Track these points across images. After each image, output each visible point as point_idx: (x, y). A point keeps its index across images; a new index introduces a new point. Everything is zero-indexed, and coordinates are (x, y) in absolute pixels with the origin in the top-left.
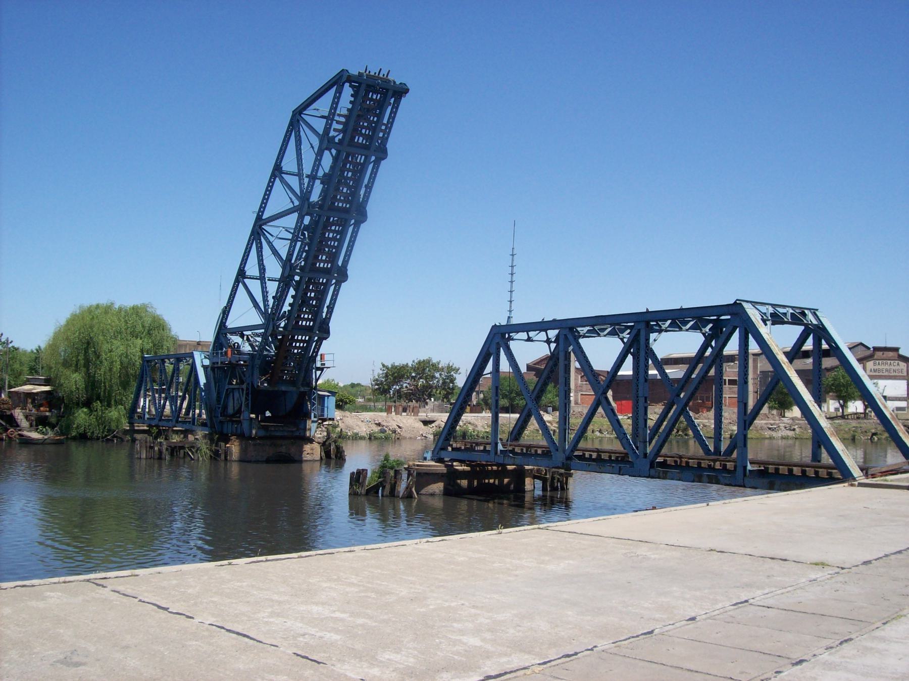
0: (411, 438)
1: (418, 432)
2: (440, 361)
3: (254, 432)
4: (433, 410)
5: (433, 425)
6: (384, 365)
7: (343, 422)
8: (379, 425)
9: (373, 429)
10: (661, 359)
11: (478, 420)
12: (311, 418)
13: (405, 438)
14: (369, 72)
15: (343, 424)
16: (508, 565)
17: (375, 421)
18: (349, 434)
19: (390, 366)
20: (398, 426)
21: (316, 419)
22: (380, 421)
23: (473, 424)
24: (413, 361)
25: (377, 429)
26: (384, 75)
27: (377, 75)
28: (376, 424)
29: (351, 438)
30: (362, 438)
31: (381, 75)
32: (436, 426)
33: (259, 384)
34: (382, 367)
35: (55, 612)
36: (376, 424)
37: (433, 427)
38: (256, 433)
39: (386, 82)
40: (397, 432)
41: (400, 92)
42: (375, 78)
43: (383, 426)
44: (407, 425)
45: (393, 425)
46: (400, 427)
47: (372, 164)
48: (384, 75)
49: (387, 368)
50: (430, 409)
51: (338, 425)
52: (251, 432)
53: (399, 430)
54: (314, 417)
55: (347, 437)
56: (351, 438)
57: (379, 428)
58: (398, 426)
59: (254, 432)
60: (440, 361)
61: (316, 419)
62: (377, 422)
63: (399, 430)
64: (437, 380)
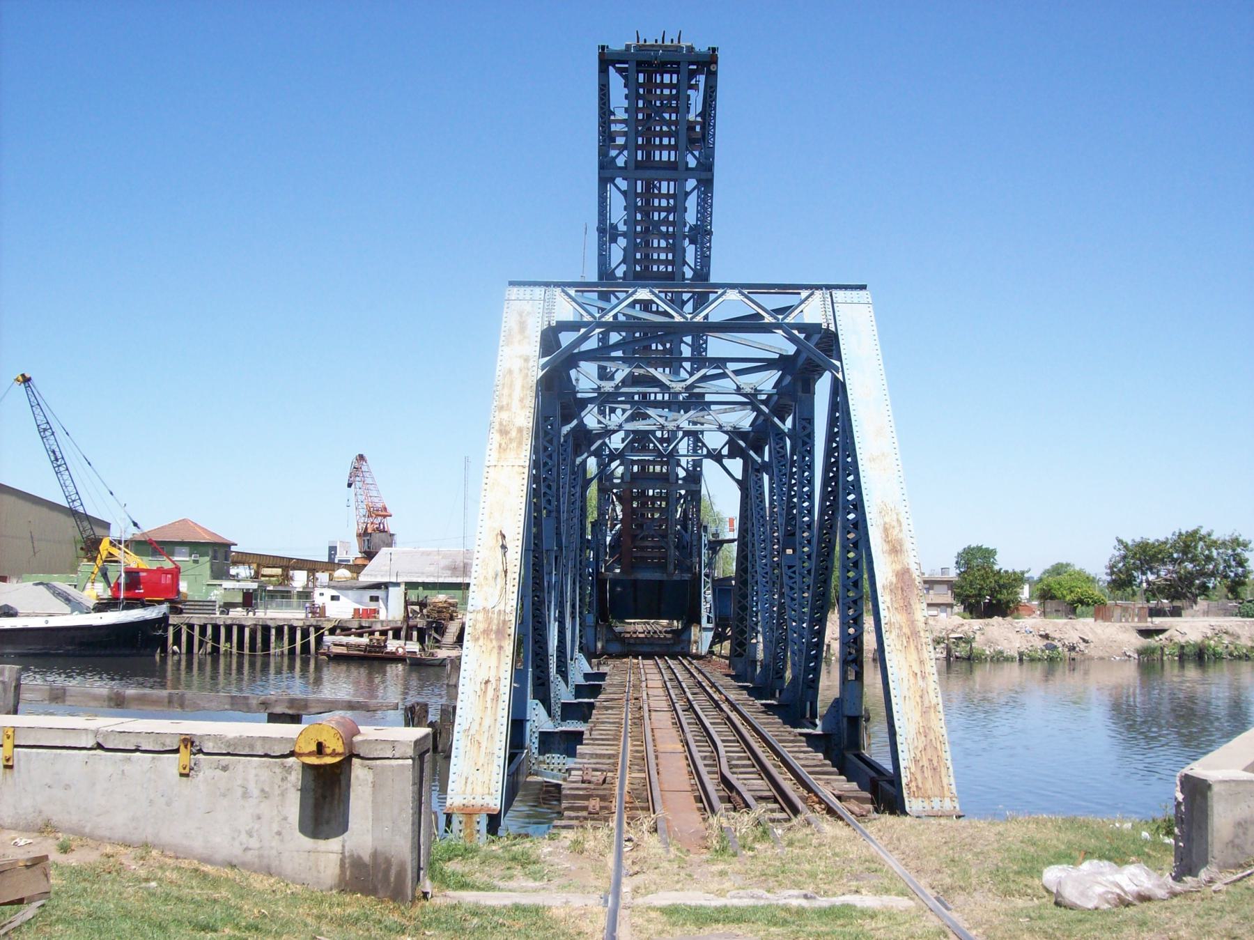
0: (1102, 659)
1: (1120, 647)
2: (1212, 531)
3: (599, 645)
4: (1208, 612)
5: (1161, 636)
6: (1120, 542)
7: (983, 634)
8: (1046, 637)
9: (1034, 644)
10: (750, 426)
11: (1243, 627)
12: (699, 622)
13: (1091, 658)
14: (645, 41)
15: (982, 637)
16: (845, 880)
17: (1039, 630)
18: (988, 653)
19: (1130, 543)
20: (1081, 638)
21: (710, 626)
22: (1047, 632)
23: (1232, 635)
24: (1173, 535)
25: (1040, 643)
26: (672, 41)
27: (660, 42)
28: (1041, 636)
29: (989, 659)
30: (1009, 659)
31: (667, 43)
32: (1166, 639)
33: (603, 570)
34: (1116, 543)
35: (732, 914)
36: (1041, 636)
37: (1161, 640)
38: (603, 647)
39: (676, 51)
40: (1077, 649)
41: (707, 63)
42: (647, 48)
43: (1054, 639)
44: (1103, 637)
45: (1073, 637)
46: (1084, 641)
47: (694, 195)
48: (672, 41)
49: (1126, 547)
50: (1202, 611)
51: (974, 638)
52: (596, 646)
53: (1082, 646)
54: (708, 622)
55: (983, 657)
56: (989, 659)
57: (1046, 642)
58: (1081, 638)
59: (599, 645)
60: (1212, 531)
61: (710, 626)
62: (1043, 633)
63: (1082, 646)
64: (1213, 563)
